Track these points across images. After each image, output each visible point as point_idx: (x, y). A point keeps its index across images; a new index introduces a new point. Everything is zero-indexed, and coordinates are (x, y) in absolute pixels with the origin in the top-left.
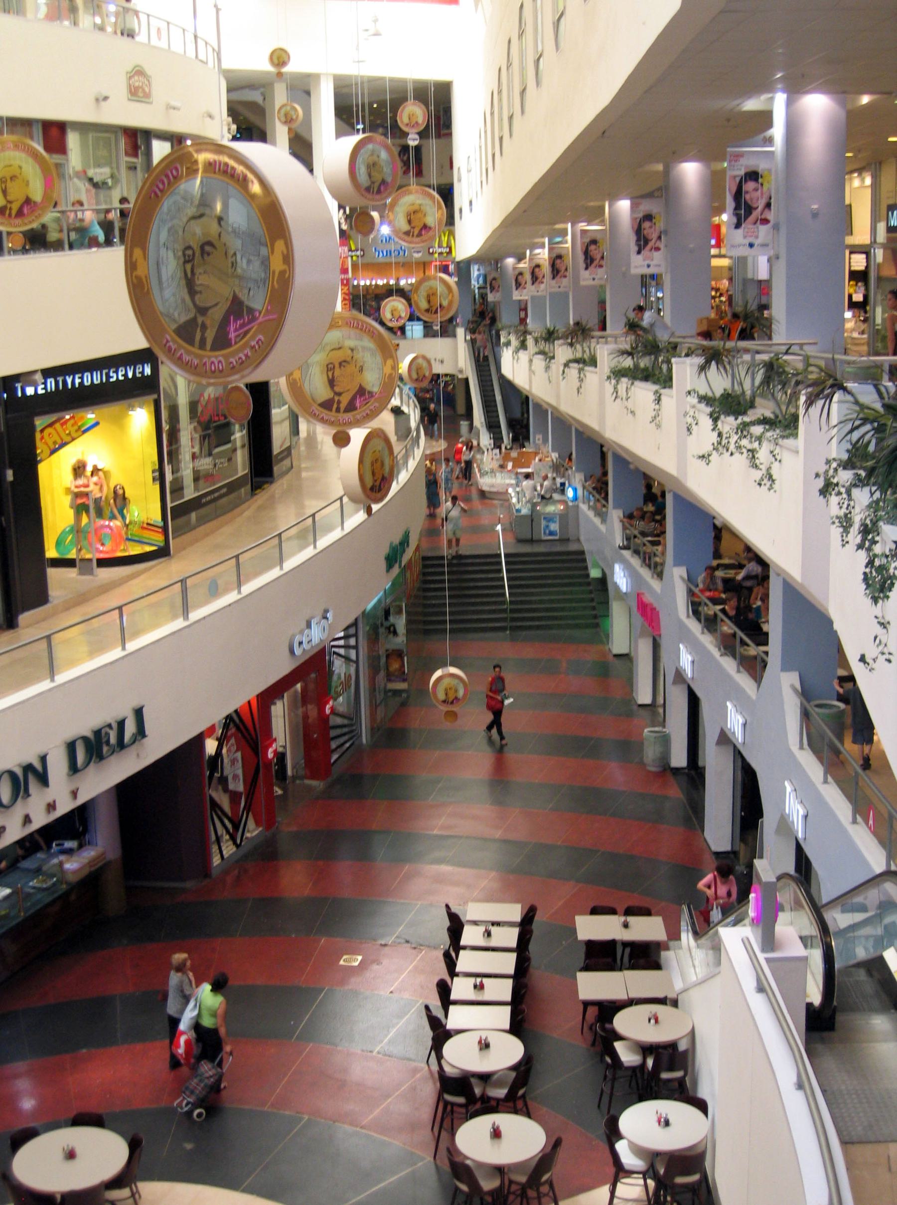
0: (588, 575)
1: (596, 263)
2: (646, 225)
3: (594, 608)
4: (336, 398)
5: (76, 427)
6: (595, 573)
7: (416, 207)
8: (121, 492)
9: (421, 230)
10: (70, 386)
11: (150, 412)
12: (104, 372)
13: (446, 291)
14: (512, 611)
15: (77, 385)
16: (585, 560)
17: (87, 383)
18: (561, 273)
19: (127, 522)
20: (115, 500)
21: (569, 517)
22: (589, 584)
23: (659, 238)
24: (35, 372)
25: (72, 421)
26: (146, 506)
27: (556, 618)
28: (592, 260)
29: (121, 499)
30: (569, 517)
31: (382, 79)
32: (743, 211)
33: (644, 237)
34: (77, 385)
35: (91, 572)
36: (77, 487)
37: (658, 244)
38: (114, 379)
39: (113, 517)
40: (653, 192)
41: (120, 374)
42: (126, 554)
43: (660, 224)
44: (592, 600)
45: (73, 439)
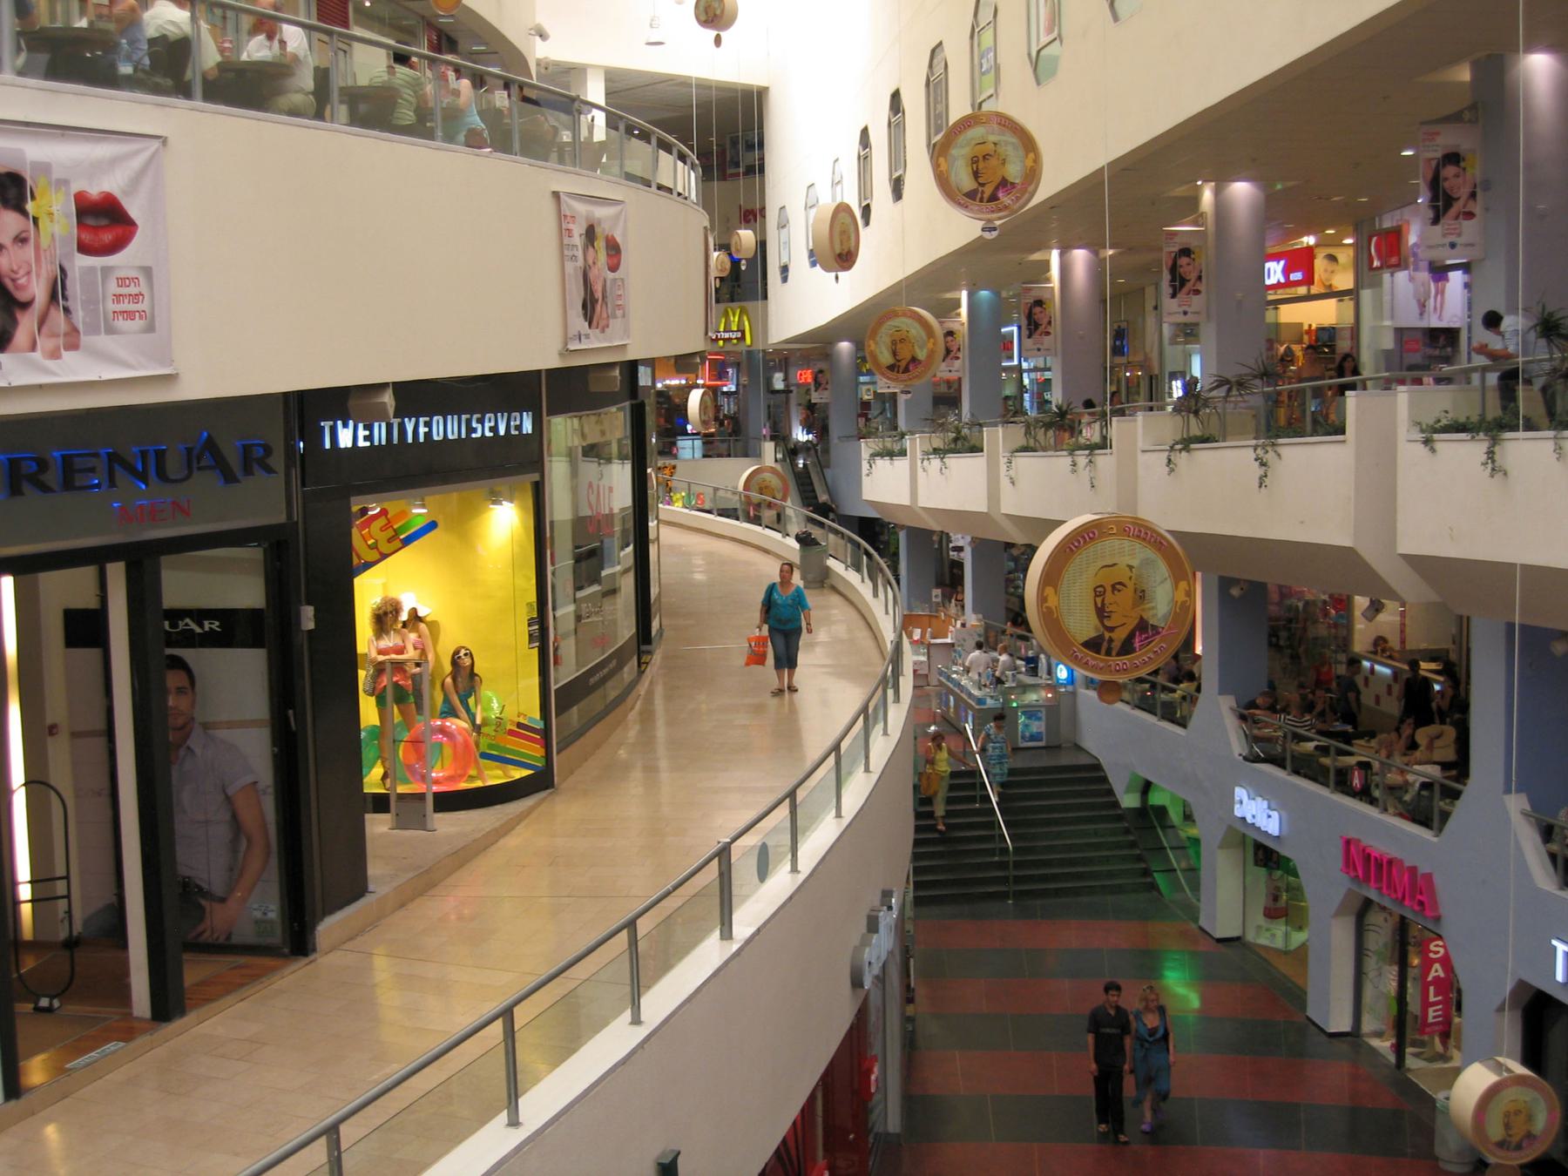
0: (1116, 804)
1: (1189, 286)
2: (1449, 171)
3: (1139, 859)
4: (1107, 635)
5: (390, 533)
6: (1129, 801)
7: (990, 148)
8: (467, 661)
9: (997, 188)
10: (410, 440)
11: (523, 508)
12: (464, 417)
13: (923, 334)
14: (1017, 865)
15: (422, 439)
16: (1104, 780)
17: (437, 436)
18: (1041, 329)
19: (478, 721)
20: (454, 680)
21: (1061, 711)
22: (1120, 818)
23: (1473, 195)
24: (384, 386)
25: (382, 521)
26: (511, 694)
27: (1080, 876)
28: (1183, 282)
29: (465, 676)
30: (1061, 711)
31: (684, 83)
32: (1179, 283)
33: (1445, 192)
34: (422, 439)
35: (422, 824)
36: (380, 652)
37: (1471, 207)
38: (478, 435)
39: (451, 712)
40: (1461, 112)
41: (487, 425)
42: (479, 784)
43: (1475, 170)
44: (1133, 845)
45: (384, 556)
